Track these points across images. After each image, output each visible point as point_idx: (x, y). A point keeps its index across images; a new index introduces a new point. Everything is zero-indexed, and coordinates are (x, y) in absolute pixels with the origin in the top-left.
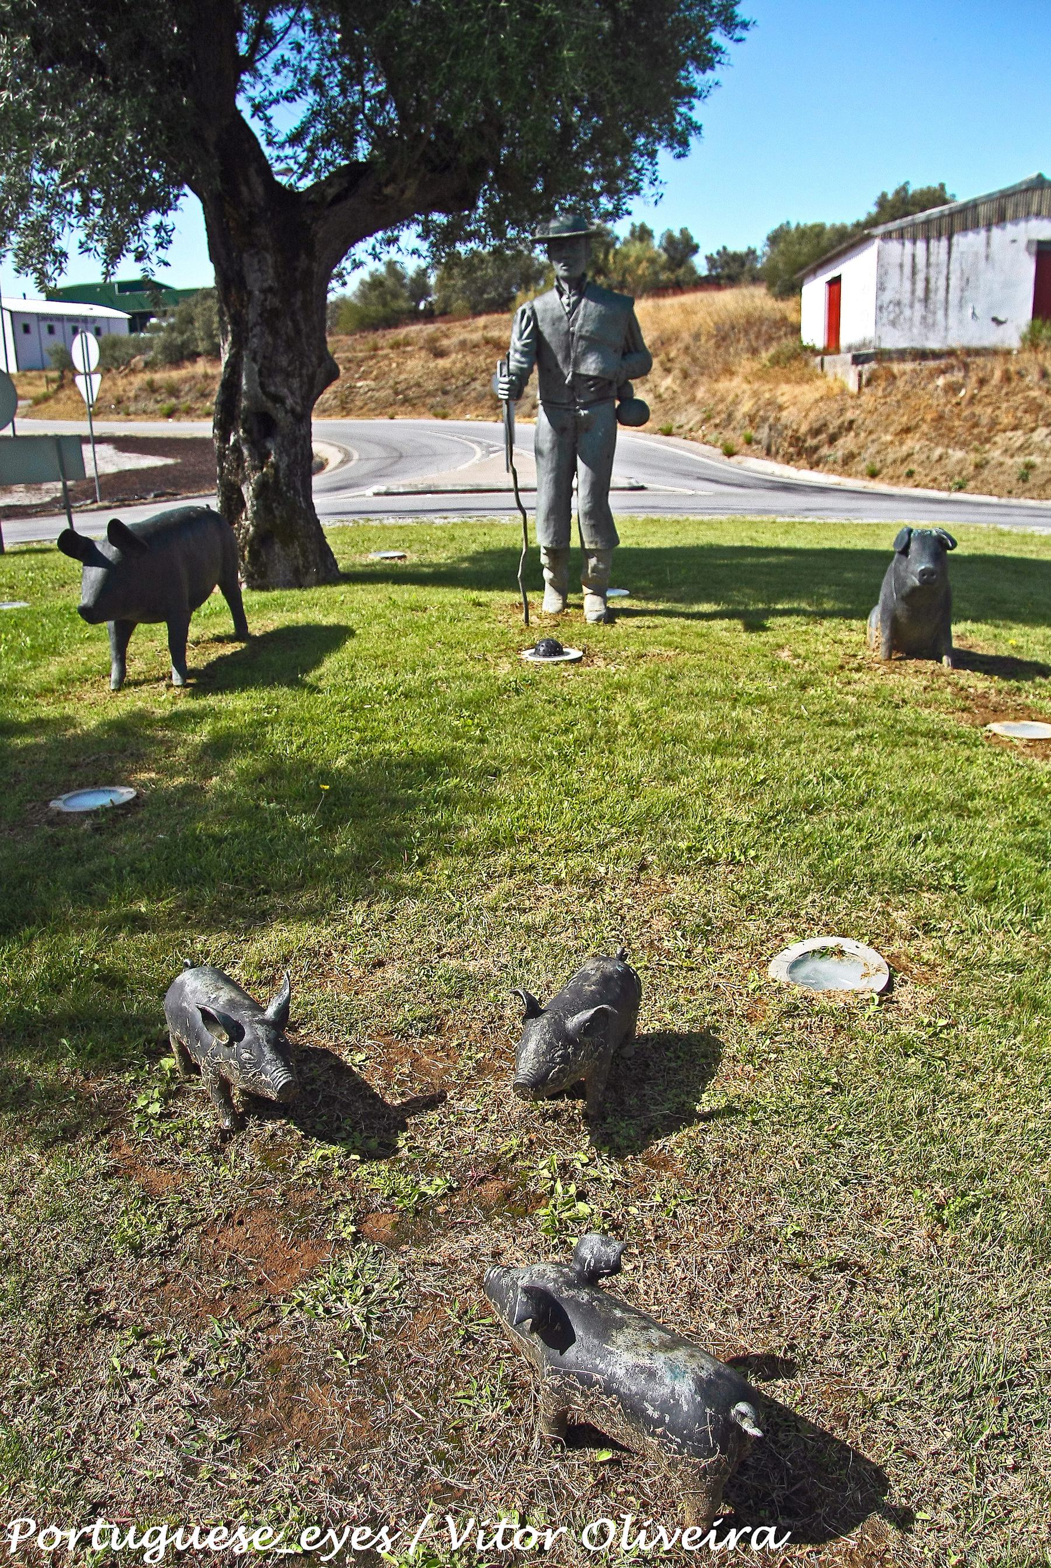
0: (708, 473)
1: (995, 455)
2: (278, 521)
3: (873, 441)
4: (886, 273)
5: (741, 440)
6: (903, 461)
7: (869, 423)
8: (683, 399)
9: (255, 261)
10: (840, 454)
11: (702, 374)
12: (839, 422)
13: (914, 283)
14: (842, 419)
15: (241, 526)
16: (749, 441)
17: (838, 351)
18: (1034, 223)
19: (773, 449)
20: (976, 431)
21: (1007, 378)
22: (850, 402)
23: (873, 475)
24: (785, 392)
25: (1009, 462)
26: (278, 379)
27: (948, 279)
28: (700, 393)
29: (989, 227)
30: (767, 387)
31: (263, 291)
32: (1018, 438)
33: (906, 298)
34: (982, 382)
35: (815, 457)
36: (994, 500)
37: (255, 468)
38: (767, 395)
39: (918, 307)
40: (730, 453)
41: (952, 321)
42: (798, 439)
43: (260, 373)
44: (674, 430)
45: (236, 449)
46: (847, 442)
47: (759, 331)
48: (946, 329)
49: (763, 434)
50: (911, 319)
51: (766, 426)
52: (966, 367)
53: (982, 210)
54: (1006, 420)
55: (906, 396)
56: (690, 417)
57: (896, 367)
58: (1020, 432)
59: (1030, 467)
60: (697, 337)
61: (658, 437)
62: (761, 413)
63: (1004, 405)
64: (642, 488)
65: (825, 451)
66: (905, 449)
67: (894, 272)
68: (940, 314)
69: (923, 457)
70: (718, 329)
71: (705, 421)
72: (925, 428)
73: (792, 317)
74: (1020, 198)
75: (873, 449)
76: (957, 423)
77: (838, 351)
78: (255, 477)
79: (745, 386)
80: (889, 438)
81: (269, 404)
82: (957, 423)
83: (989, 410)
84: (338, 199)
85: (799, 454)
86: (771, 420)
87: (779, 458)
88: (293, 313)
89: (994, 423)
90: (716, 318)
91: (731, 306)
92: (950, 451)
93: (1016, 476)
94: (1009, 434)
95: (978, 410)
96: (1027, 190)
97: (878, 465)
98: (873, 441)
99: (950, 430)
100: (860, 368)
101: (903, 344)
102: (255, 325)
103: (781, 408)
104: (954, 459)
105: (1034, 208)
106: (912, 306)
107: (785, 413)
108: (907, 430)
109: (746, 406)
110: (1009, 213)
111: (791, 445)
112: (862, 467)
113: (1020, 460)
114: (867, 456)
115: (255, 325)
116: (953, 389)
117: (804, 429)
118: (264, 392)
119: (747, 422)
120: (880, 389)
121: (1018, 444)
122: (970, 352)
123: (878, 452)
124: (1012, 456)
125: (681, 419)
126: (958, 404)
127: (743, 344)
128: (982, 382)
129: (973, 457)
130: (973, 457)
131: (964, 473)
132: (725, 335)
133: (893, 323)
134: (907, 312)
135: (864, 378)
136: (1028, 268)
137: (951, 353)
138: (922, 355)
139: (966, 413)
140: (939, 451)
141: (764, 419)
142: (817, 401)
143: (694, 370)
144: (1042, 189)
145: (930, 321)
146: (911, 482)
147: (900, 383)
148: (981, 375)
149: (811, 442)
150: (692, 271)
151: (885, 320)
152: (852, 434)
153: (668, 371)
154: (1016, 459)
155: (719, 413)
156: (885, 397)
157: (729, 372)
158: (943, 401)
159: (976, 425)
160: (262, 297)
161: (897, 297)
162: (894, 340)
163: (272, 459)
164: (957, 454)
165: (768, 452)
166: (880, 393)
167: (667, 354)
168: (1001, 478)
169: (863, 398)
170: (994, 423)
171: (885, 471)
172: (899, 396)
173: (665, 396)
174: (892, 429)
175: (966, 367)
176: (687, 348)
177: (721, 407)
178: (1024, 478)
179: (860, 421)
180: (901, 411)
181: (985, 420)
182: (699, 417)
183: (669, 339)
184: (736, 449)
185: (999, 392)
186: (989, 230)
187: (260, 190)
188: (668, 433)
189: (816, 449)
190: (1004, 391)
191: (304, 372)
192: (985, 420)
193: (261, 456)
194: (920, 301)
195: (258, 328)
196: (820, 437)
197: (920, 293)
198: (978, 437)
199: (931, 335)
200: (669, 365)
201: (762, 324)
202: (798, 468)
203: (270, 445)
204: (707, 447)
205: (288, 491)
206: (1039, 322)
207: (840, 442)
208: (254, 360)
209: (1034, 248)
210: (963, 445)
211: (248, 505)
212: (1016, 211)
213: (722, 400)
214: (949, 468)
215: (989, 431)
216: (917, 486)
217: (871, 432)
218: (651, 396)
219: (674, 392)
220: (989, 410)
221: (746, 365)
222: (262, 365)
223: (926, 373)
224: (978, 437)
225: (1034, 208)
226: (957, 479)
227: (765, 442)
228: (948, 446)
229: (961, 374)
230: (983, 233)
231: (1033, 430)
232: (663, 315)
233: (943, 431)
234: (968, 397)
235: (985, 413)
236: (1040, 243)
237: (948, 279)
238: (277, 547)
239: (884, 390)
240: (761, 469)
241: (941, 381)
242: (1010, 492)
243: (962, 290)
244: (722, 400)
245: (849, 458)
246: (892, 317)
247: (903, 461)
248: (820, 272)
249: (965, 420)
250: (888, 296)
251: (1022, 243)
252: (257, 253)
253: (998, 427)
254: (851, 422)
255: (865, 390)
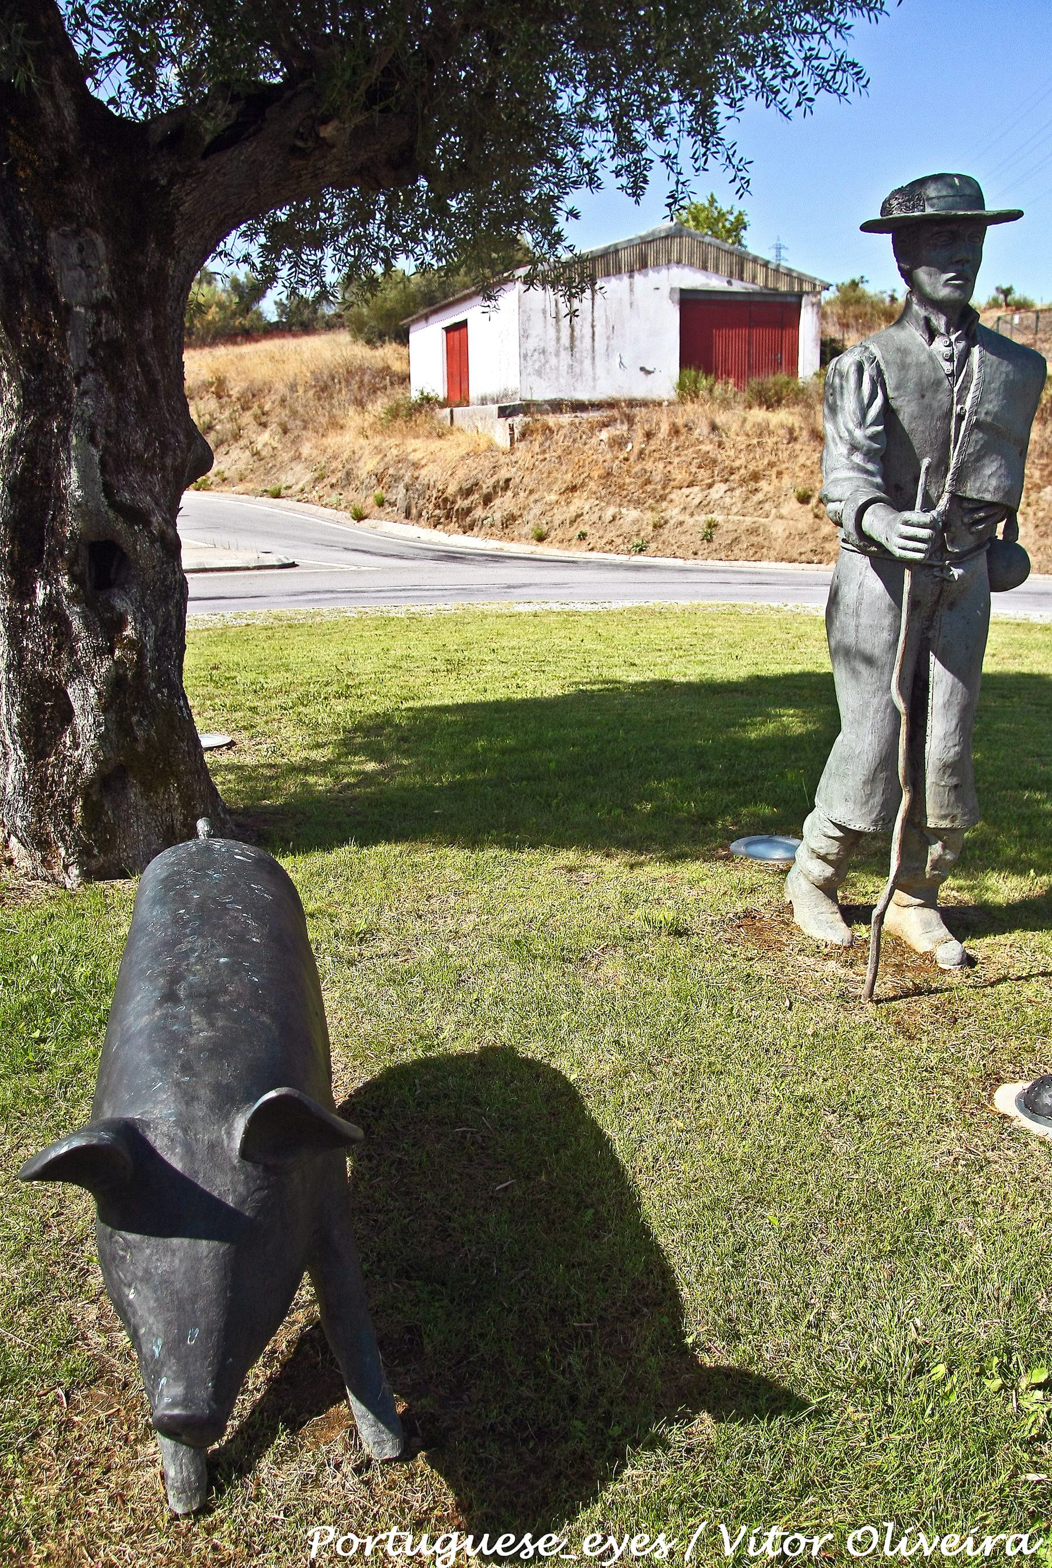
0: (352, 543)
1: (673, 513)
2: (140, 748)
3: (536, 501)
4: (529, 319)
5: (371, 500)
6: (572, 522)
7: (529, 481)
8: (286, 457)
9: (73, 249)
10: (498, 516)
11: (305, 428)
12: (491, 482)
13: (558, 331)
14: (495, 478)
15: (63, 760)
16: (381, 503)
17: (465, 402)
18: (675, 270)
19: (414, 511)
20: (649, 488)
21: (675, 431)
22: (503, 460)
23: (541, 538)
24: (418, 447)
25: (690, 521)
26: (134, 477)
27: (593, 327)
28: (306, 450)
29: (631, 272)
30: (392, 441)
31: (98, 306)
32: (696, 494)
33: (551, 346)
34: (649, 435)
35: (468, 519)
36: (679, 563)
37: (99, 652)
38: (394, 451)
39: (565, 355)
40: (359, 517)
41: (600, 371)
42: (446, 500)
43: (103, 463)
44: (283, 492)
45: (53, 613)
46: (504, 504)
47: (362, 381)
48: (594, 379)
49: (399, 494)
50: (557, 369)
51: (401, 485)
52: (630, 420)
53: (624, 255)
54: (680, 476)
55: (568, 451)
56: (298, 476)
57: (551, 420)
58: (696, 489)
59: (712, 525)
60: (293, 388)
61: (264, 499)
62: (391, 471)
63: (676, 460)
64: (293, 565)
65: (479, 513)
66: (572, 510)
67: (537, 318)
68: (587, 362)
69: (595, 518)
70: (317, 380)
71: (320, 479)
72: (592, 485)
73: (397, 366)
74: (660, 244)
75: (536, 510)
76: (628, 480)
77: (465, 402)
78: (103, 667)
79: (362, 441)
80: (553, 497)
81: (120, 526)
82: (628, 480)
83: (661, 465)
84: (223, 143)
85: (448, 517)
86: (407, 479)
87: (423, 521)
88: (141, 351)
89: (667, 480)
90: (312, 367)
91: (327, 354)
92: (624, 511)
93: (700, 536)
94: (686, 491)
95: (649, 465)
96: (666, 237)
97: (545, 528)
98: (536, 501)
99: (621, 487)
100: (510, 420)
101: (551, 395)
102: (83, 372)
103: (416, 466)
104: (629, 519)
105: (675, 256)
106: (557, 355)
107: (423, 472)
108: (573, 489)
109: (369, 465)
110: (651, 260)
111: (437, 506)
112: (525, 530)
113: (702, 518)
114: (530, 518)
115: (83, 372)
116: (618, 443)
117: (452, 489)
118: (114, 505)
119: (374, 481)
120: (537, 443)
121: (696, 502)
122: (632, 403)
123: (543, 514)
124: (692, 515)
125: (286, 479)
126: (626, 459)
127: (345, 395)
128: (649, 435)
129: (650, 517)
130: (650, 517)
131: (642, 534)
132: (324, 387)
133: (539, 373)
134: (553, 361)
135: (516, 431)
136: (672, 317)
137: (612, 405)
138: (579, 407)
139: (637, 468)
140: (611, 511)
141: (397, 479)
142: (463, 458)
143: (295, 424)
144: (681, 237)
145: (578, 370)
146: (584, 544)
147: (559, 437)
148: (647, 427)
149: (461, 504)
150: (260, 315)
151: (530, 370)
152: (509, 493)
153: (264, 425)
154: (696, 517)
155: (333, 472)
156: (544, 452)
157: (336, 425)
158: (609, 456)
159: (648, 482)
160: (93, 319)
161: (542, 345)
162: (543, 392)
163: (129, 632)
164: (631, 514)
165: (408, 515)
166: (537, 449)
167: (261, 407)
168: (683, 538)
169: (518, 454)
170: (667, 480)
171: (553, 534)
172: (559, 452)
173: (264, 453)
174: (556, 488)
175: (630, 420)
176: (283, 400)
177: (334, 464)
178: (708, 538)
179: (518, 480)
180: (564, 468)
181: (657, 477)
182: (309, 476)
183: (261, 391)
184: (366, 512)
185: (668, 446)
186: (631, 277)
187: (69, 114)
188: (277, 495)
189: (469, 510)
190: (674, 445)
191: (169, 461)
192: (657, 477)
193: (108, 627)
194: (565, 349)
195: (91, 376)
196: (471, 498)
197: (565, 340)
198: (652, 494)
199: (578, 385)
200: (264, 419)
201: (364, 374)
202: (449, 533)
203: (122, 604)
204: (329, 511)
205: (159, 689)
206: (686, 372)
207: (497, 502)
208: (92, 439)
209: (677, 296)
210: (638, 503)
211: (83, 722)
212: (657, 258)
213: (335, 457)
214: (625, 529)
215: (664, 488)
216: (592, 549)
217: (531, 492)
218: (248, 453)
219: (274, 449)
220: (661, 465)
221: (354, 419)
222: (106, 449)
223: (585, 426)
224: (652, 494)
225: (675, 256)
226: (636, 541)
227: (401, 504)
228: (620, 505)
229: (625, 427)
230: (625, 278)
231: (710, 486)
232: (247, 363)
233: (613, 488)
234: (636, 451)
235: (657, 469)
236: (682, 291)
237: (593, 327)
238: (134, 794)
239: (541, 445)
240: (403, 534)
241: (604, 435)
242: (696, 554)
243: (608, 338)
244: (335, 457)
245: (510, 520)
246: (537, 366)
247: (572, 522)
248: (432, 319)
249: (636, 476)
250: (532, 344)
251: (665, 291)
252: (77, 233)
253: (672, 483)
254: (508, 481)
255: (521, 445)
